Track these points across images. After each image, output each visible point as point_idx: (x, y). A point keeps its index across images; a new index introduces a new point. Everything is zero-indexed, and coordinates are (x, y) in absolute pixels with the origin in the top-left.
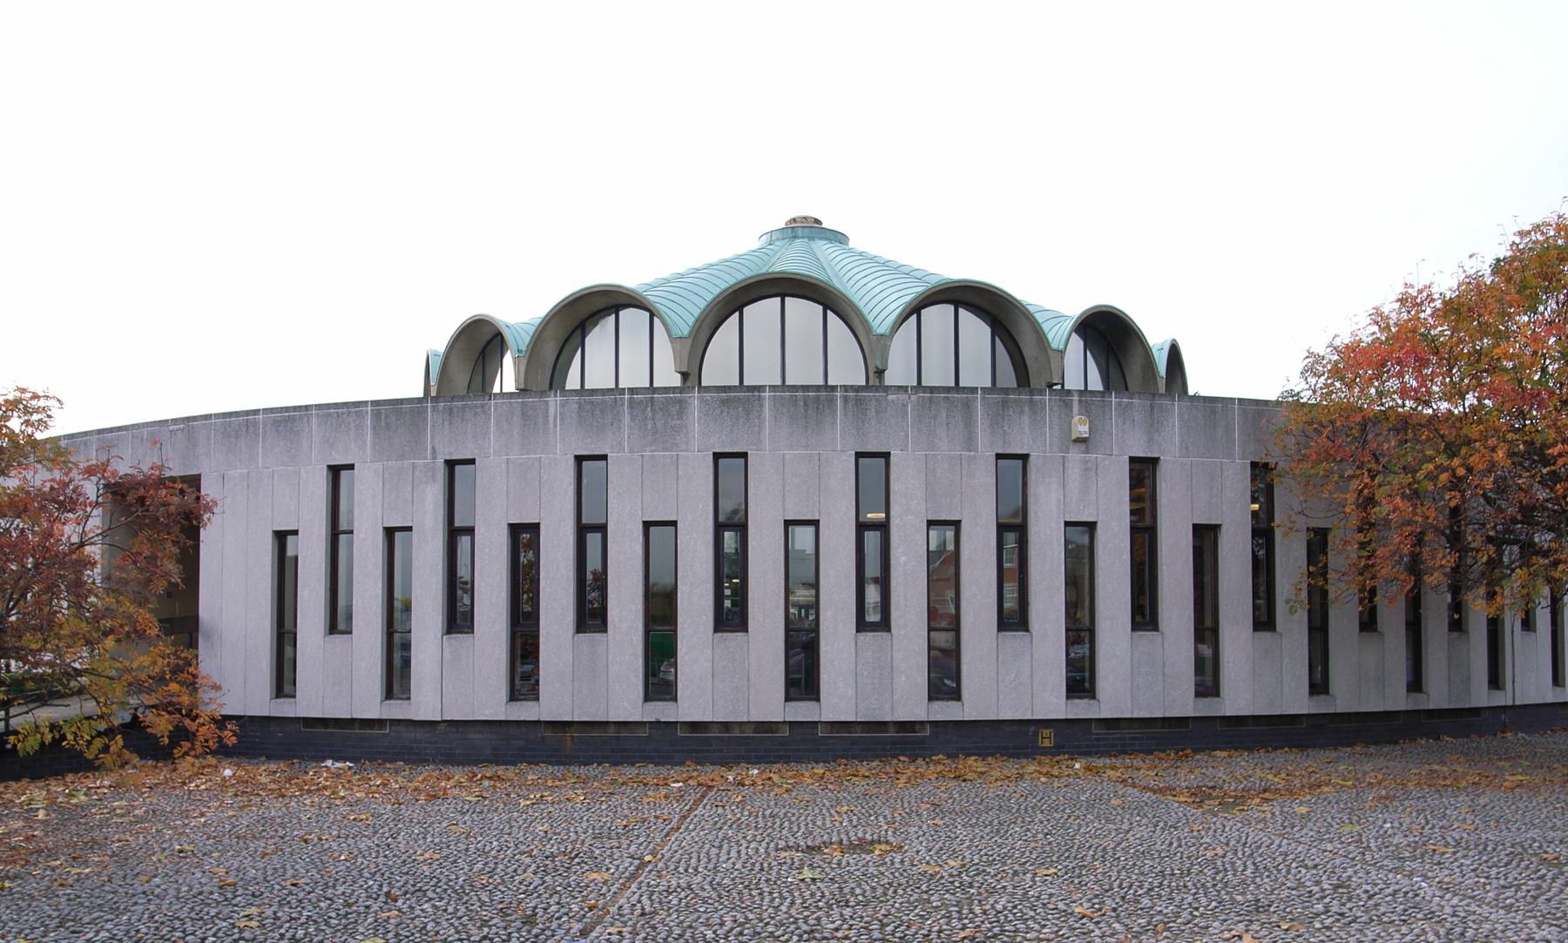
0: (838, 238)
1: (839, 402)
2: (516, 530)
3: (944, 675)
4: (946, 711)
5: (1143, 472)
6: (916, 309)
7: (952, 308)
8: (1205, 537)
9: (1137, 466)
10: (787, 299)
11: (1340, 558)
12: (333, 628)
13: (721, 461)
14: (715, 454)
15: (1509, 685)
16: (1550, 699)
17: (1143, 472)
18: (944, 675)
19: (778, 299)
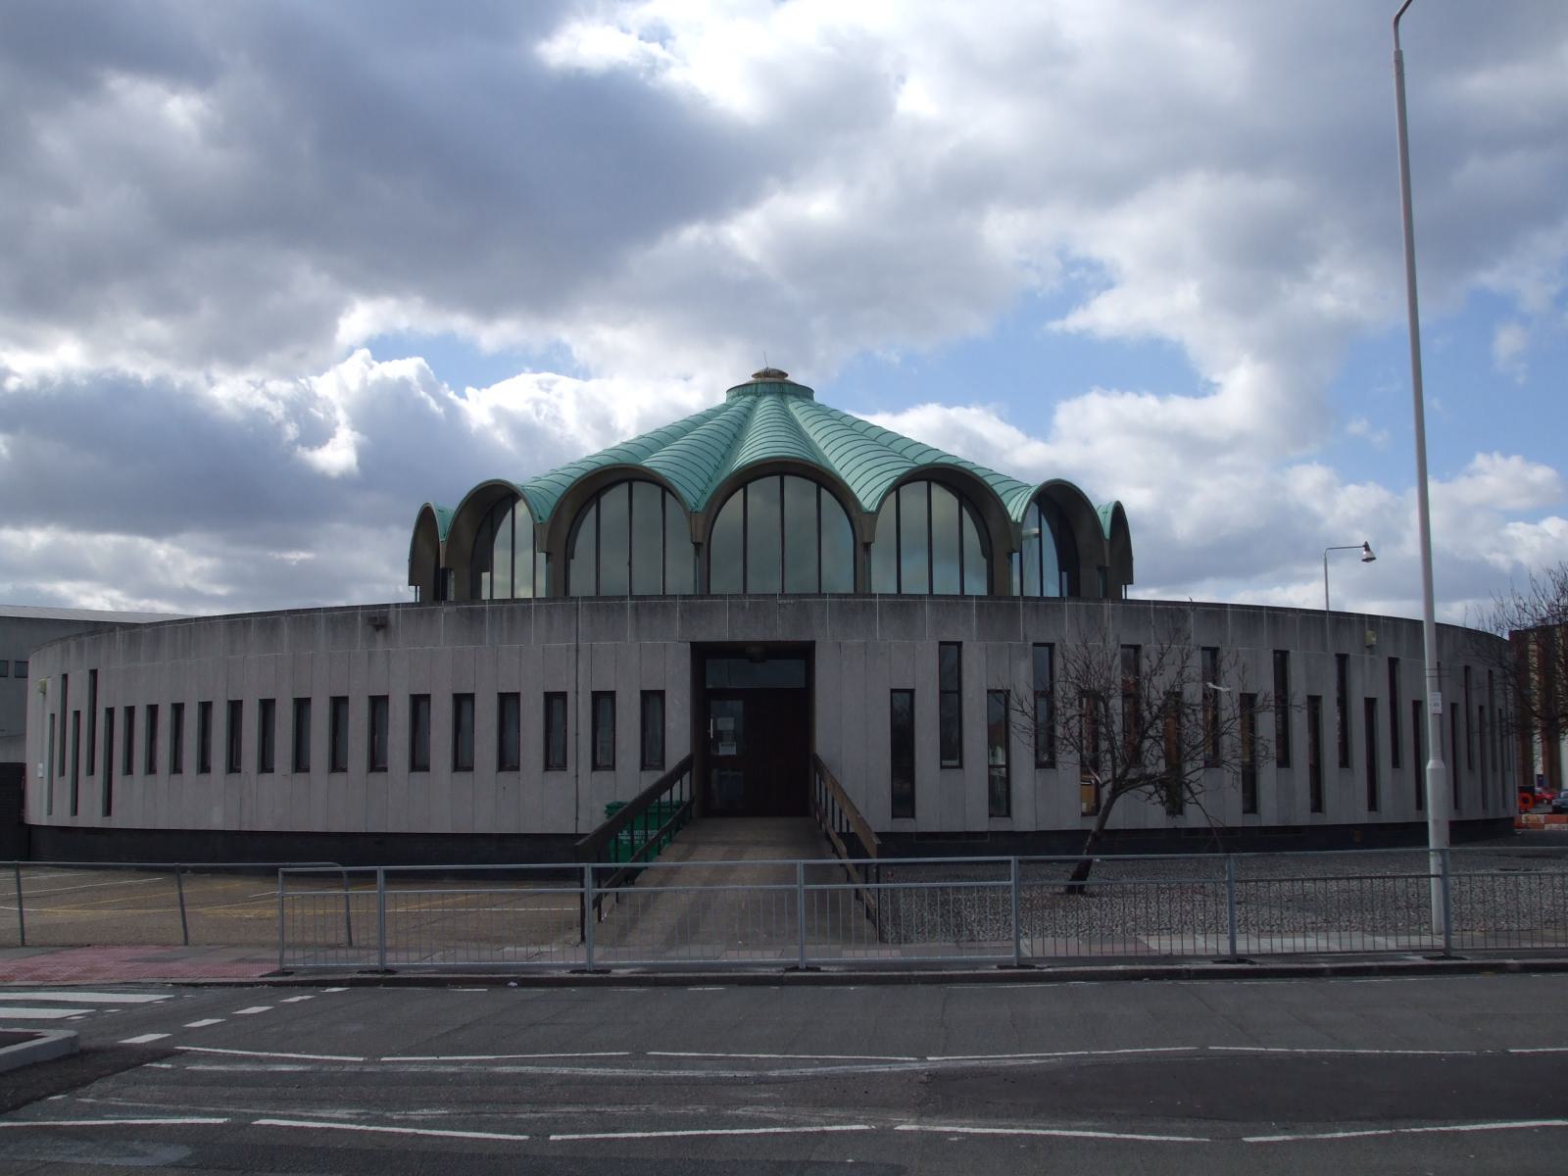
0: (804, 393)
1: (1367, 624)
2: (646, 695)
3: (1000, 799)
4: (1002, 825)
5: (1281, 659)
6: (896, 487)
7: (924, 484)
8: (1370, 704)
9: (1125, 650)
10: (787, 479)
11: (1267, 724)
12: (458, 766)
13: (955, 647)
14: (1054, 644)
15: (1517, 789)
16: (1365, 820)
17: (1281, 659)
18: (1000, 799)
19: (777, 479)
